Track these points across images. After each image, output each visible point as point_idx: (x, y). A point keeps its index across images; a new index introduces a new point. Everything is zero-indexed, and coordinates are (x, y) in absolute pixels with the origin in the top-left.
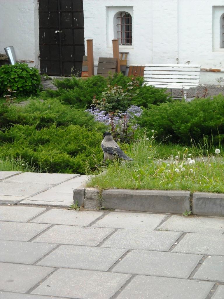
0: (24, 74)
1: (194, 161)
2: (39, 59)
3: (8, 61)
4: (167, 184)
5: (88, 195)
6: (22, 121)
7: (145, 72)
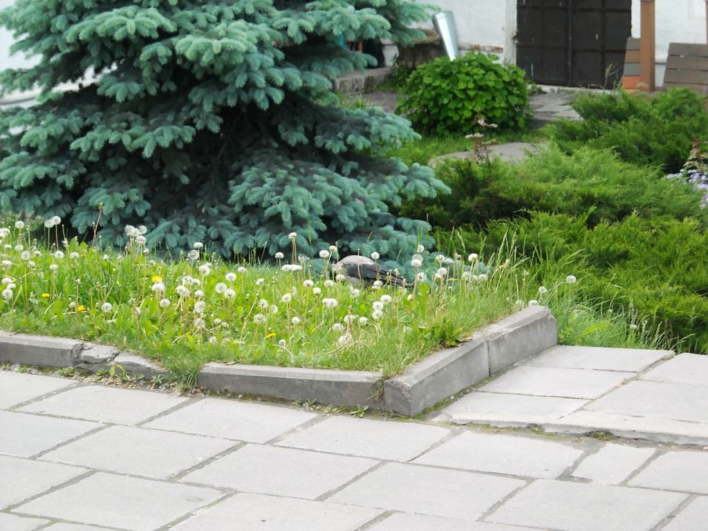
0: (490, 80)
2: (514, 43)
3: (439, 47)
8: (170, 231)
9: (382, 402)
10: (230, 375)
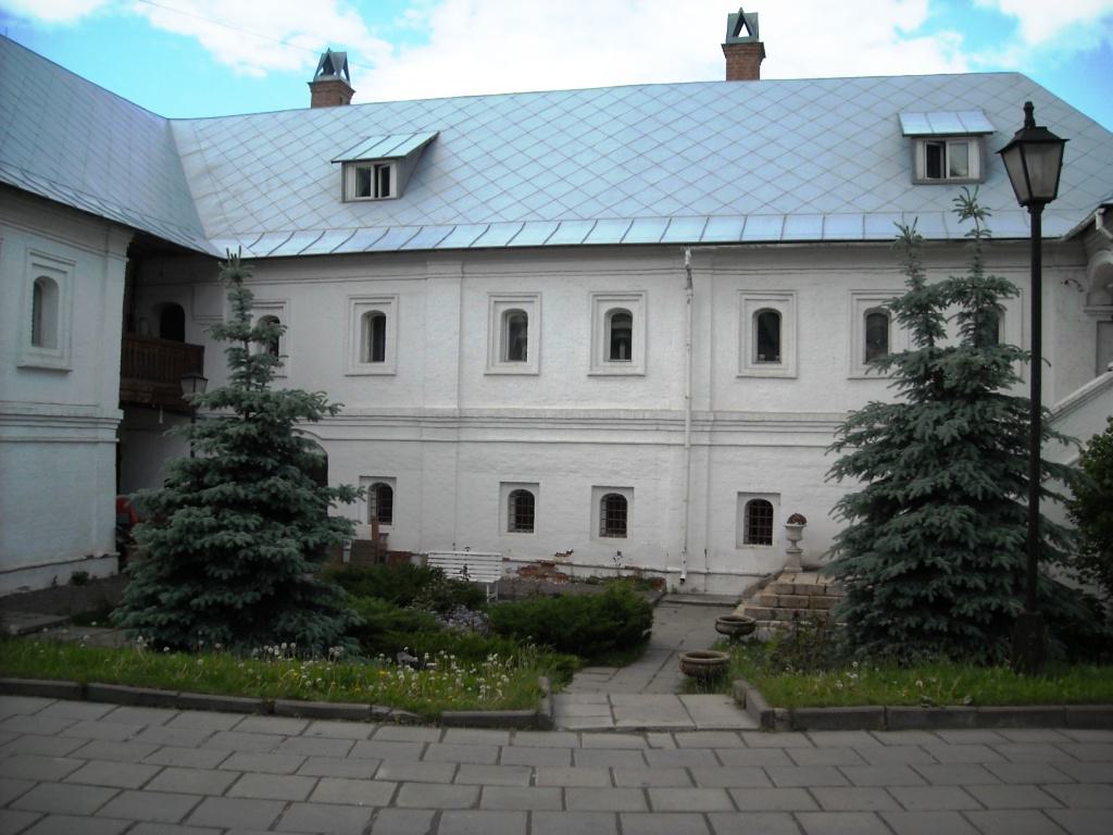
1: (342, 648)
5: (779, 716)
7: (116, 427)
10: (986, 721)
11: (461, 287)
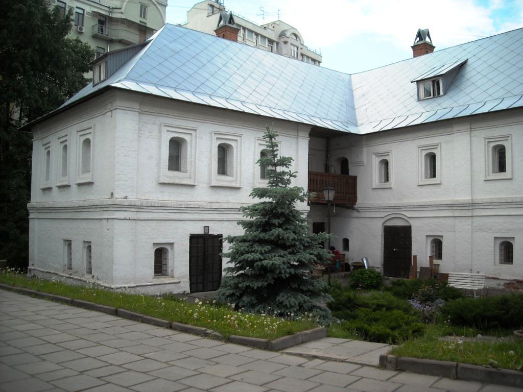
3: (364, 266)
4: (443, 356)
5: (389, 360)
6: (365, 305)
7: (449, 278)
8: (261, 307)
9: (267, 347)
11: (470, 137)
